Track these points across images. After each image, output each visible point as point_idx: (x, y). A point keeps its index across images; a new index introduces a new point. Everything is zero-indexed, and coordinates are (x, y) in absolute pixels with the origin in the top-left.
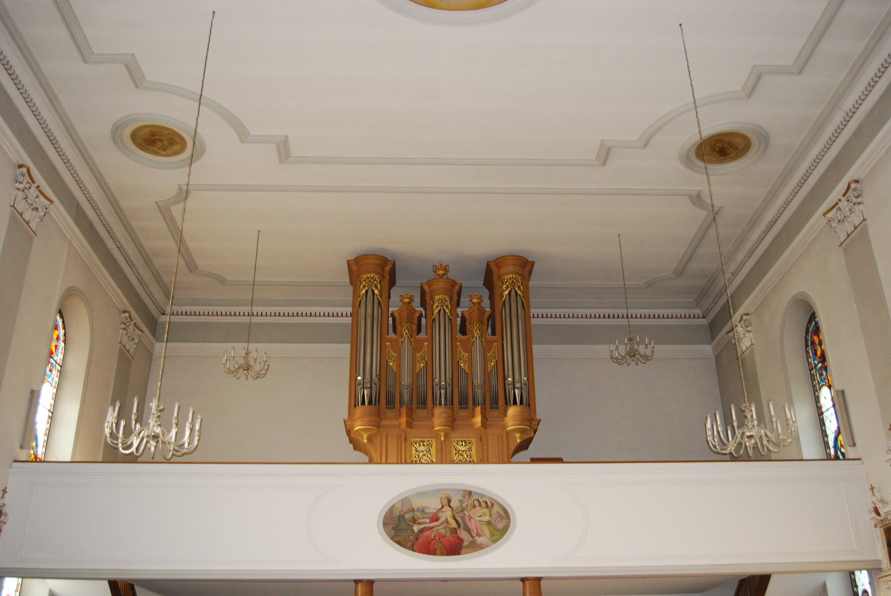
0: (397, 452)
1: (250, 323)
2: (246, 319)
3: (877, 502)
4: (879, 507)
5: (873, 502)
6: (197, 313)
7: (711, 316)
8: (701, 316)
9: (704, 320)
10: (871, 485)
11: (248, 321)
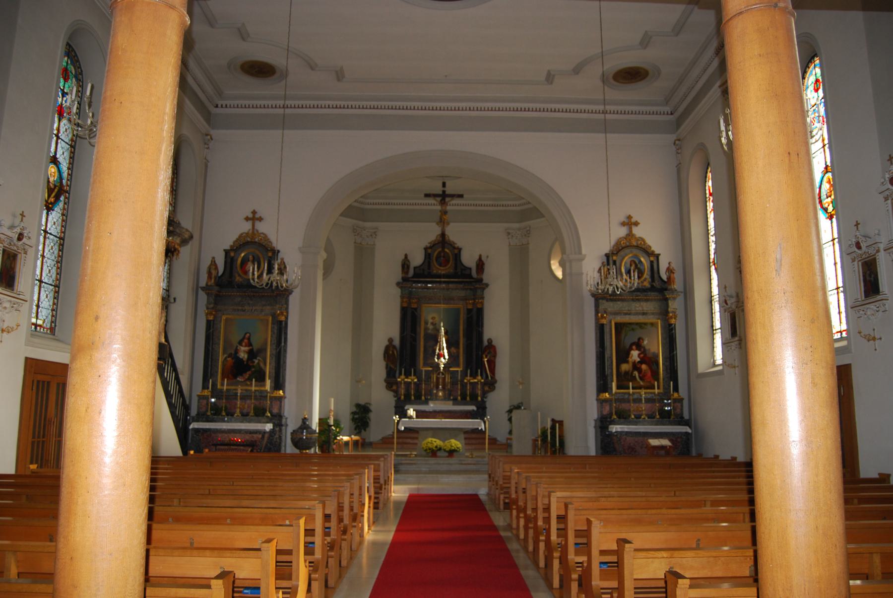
0: (31, 408)
1: (605, 119)
2: (281, 111)
3: (860, 237)
4: (862, 241)
5: (856, 236)
6: (449, 109)
7: (677, 114)
8: (669, 113)
9: (672, 116)
10: (857, 221)
11: (283, 112)
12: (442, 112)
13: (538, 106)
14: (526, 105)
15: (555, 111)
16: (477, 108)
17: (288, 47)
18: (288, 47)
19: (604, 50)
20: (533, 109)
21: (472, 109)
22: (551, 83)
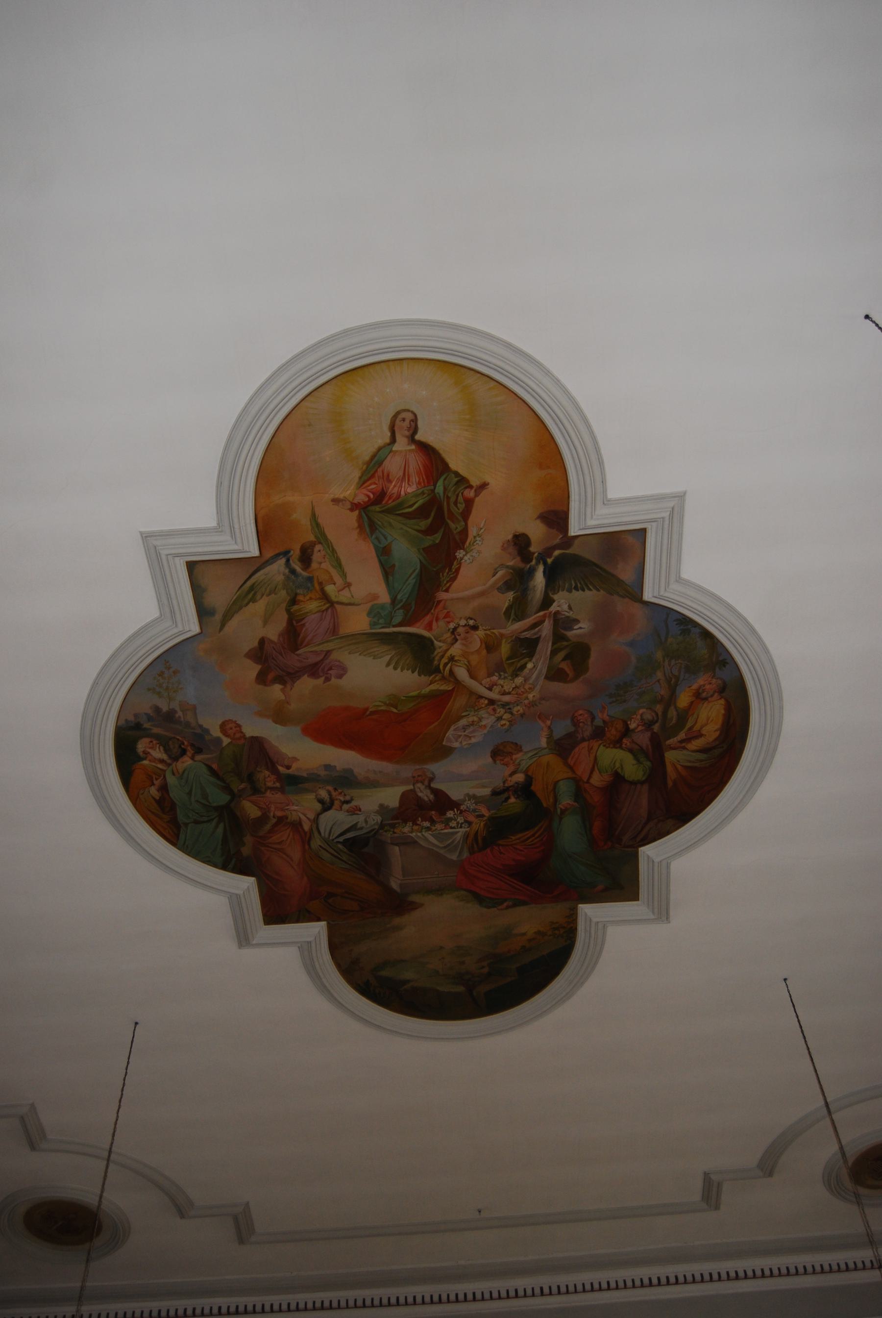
12: (462, 1308)
13: (696, 1268)
14: (670, 1270)
15: (737, 1277)
16: (542, 1289)
17: (110, 1152)
18: (110, 1152)
19: (843, 1143)
20: (676, 1278)
21: (546, 1291)
22: (717, 1207)
